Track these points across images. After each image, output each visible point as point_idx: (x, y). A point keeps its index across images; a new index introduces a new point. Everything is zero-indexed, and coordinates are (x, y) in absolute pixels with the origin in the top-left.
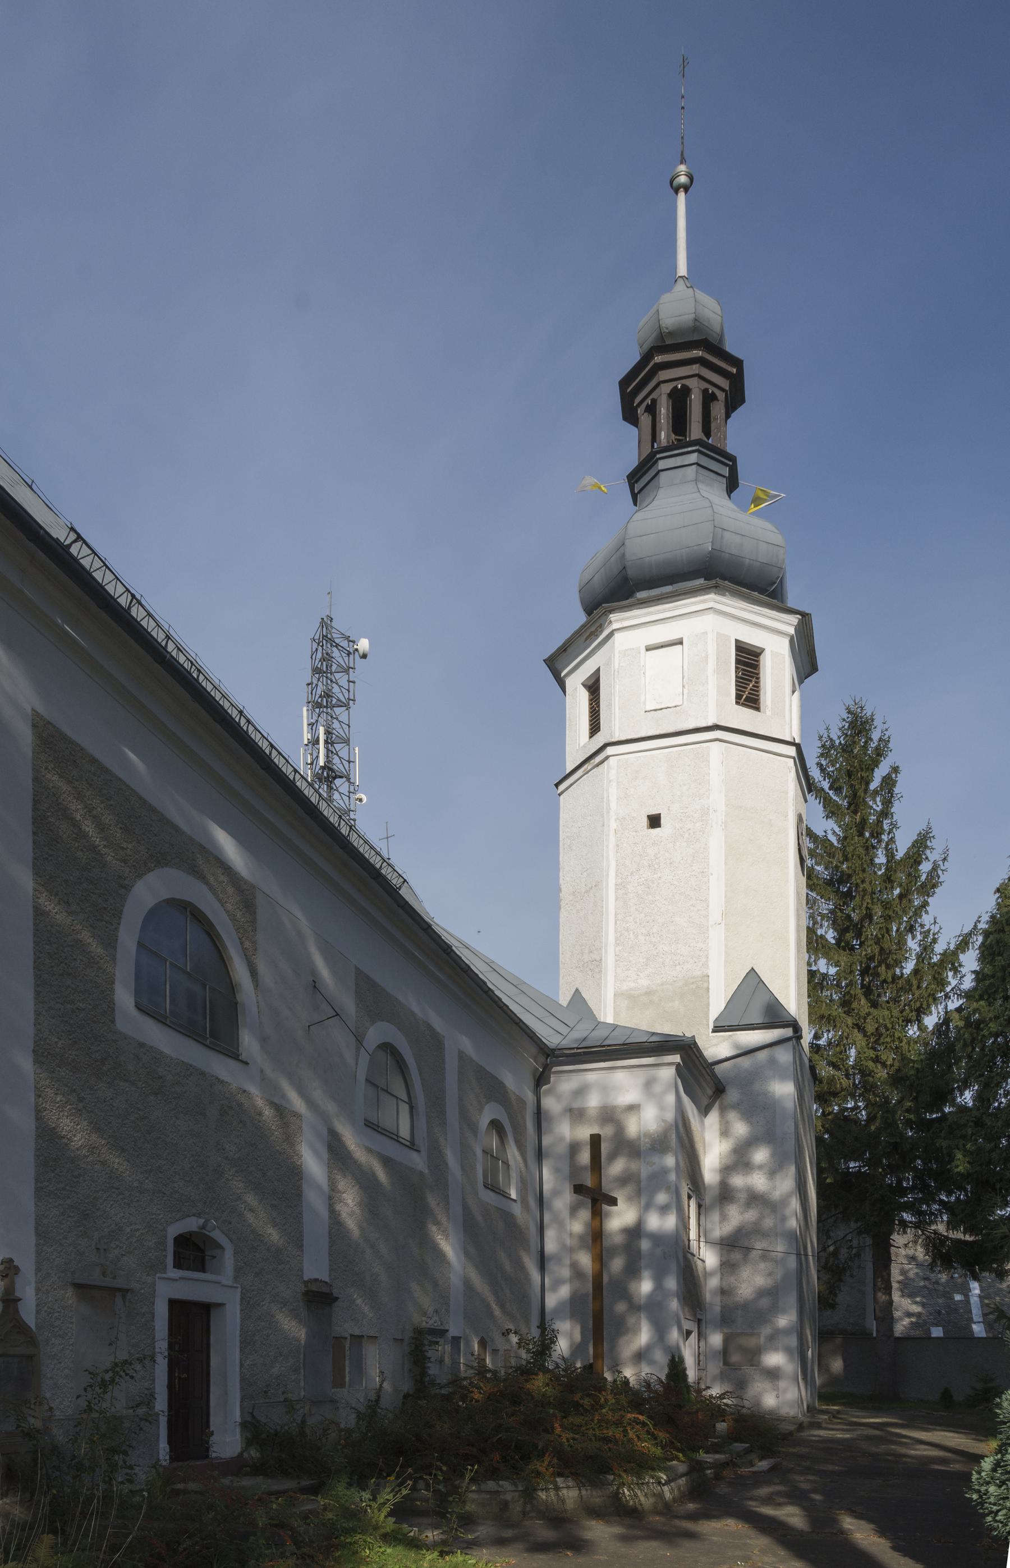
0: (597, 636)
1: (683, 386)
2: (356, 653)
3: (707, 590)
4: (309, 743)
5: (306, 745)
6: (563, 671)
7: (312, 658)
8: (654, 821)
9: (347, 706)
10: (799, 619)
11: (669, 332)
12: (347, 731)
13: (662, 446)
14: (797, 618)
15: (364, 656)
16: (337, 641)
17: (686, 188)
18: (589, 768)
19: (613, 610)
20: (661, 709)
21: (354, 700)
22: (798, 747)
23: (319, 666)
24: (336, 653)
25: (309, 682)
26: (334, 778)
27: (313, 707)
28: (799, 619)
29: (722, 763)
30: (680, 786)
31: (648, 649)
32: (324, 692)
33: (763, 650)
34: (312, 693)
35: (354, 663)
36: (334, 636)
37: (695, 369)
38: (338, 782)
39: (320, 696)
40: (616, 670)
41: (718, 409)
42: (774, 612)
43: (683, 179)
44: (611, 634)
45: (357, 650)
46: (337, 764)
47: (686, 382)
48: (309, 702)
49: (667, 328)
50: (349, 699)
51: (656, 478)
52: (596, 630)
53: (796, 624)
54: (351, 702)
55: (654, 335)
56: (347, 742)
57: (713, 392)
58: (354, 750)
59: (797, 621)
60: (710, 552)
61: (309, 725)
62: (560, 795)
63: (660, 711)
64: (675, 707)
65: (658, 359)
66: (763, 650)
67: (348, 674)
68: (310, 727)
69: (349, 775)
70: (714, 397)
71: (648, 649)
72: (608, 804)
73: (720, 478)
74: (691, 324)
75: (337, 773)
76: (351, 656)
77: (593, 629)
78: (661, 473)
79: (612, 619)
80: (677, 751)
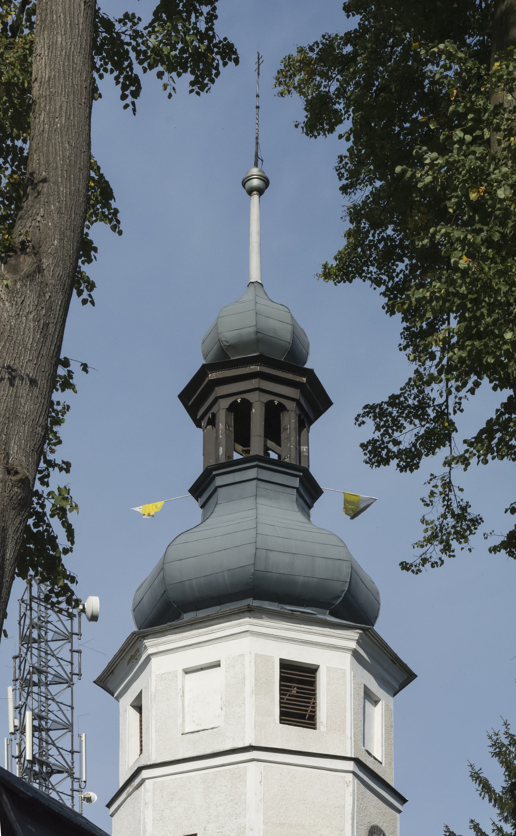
0: (138, 660)
1: (243, 400)
2: (83, 615)
3: (241, 615)
5: (12, 734)
6: (116, 691)
7: (20, 624)
9: (70, 683)
10: (360, 634)
11: (229, 345)
12: (68, 714)
13: (220, 462)
14: (358, 633)
15: (94, 618)
17: (260, 191)
18: (131, 790)
19: (147, 636)
20: (198, 731)
21: (79, 675)
22: (357, 761)
23: (28, 634)
24: (53, 617)
25: (17, 654)
28: (360, 634)
29: (260, 782)
30: (217, 806)
31: (187, 672)
32: (33, 667)
33: (318, 666)
34: (20, 668)
35: (80, 627)
37: (254, 383)
38: (55, 779)
39: (29, 673)
40: (153, 694)
42: (327, 630)
43: (256, 182)
44: (148, 659)
47: (246, 396)
48: (17, 680)
49: (227, 342)
50: (72, 674)
51: (215, 495)
52: (135, 654)
53: (357, 638)
54: (75, 678)
55: (216, 347)
56: (69, 727)
57: (279, 403)
58: (80, 736)
59: (358, 635)
60: (254, 574)
61: (16, 708)
62: (112, 815)
63: (197, 733)
64: (212, 728)
65: (212, 376)
66: (318, 666)
67: (71, 642)
68: (18, 711)
69: (72, 769)
70: (282, 408)
71: (187, 672)
72: (144, 823)
73: (289, 490)
74: (253, 337)
75: (54, 767)
76: (76, 620)
77: (132, 653)
78: (219, 490)
79: (146, 644)
80: (213, 773)
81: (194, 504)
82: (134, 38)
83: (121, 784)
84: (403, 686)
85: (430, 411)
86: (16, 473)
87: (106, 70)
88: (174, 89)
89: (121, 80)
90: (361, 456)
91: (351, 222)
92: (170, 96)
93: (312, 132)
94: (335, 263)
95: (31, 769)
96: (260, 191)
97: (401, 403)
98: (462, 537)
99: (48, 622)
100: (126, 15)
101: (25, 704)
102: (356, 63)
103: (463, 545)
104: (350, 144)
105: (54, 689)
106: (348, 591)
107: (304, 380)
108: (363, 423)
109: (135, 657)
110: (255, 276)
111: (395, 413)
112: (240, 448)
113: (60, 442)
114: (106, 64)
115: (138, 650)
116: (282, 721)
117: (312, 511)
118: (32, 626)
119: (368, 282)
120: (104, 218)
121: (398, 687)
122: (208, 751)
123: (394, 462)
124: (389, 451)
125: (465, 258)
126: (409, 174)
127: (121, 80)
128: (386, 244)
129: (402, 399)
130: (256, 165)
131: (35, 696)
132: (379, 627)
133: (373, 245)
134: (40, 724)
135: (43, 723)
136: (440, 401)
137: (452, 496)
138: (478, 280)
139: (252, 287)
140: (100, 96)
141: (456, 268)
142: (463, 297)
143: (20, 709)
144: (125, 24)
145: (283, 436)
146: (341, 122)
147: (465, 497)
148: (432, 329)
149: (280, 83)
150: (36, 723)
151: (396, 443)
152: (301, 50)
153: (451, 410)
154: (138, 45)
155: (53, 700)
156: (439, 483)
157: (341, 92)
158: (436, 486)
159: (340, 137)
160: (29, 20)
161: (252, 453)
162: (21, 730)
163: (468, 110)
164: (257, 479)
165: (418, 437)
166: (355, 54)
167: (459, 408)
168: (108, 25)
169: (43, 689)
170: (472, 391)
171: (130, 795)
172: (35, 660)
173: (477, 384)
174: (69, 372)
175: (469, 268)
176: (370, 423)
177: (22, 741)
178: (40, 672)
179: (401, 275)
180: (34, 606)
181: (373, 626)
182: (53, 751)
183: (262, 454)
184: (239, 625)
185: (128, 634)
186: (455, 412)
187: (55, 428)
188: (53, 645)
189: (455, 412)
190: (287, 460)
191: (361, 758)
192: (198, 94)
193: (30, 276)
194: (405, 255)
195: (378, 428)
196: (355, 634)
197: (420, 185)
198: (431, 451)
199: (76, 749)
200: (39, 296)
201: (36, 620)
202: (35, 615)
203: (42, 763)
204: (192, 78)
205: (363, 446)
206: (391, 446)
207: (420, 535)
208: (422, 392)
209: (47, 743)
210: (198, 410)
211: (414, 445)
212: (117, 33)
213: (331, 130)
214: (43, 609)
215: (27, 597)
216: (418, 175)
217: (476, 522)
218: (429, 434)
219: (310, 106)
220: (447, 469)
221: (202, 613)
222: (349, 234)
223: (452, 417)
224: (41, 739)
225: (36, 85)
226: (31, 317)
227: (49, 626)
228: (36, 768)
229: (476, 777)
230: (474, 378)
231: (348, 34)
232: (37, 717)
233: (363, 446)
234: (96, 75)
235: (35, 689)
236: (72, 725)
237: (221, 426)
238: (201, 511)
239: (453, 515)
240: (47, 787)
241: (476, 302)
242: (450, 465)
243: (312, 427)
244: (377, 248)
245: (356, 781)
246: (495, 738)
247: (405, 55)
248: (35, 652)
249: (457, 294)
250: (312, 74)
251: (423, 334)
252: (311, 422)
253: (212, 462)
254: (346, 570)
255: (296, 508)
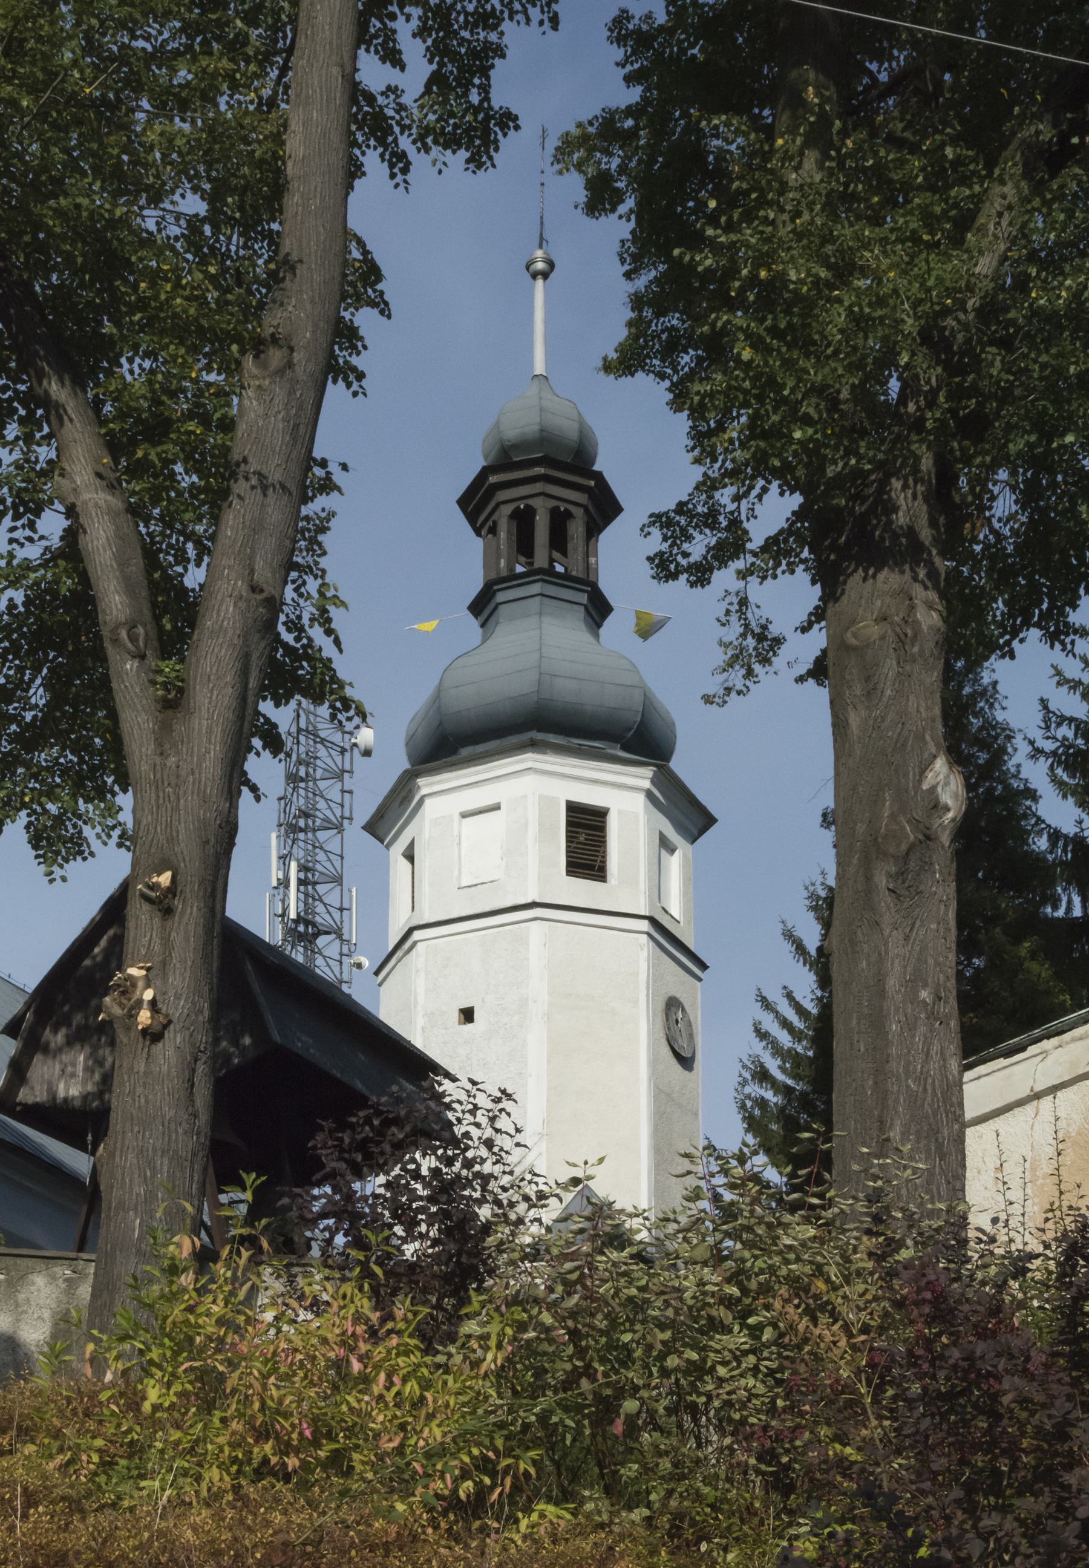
0: (410, 802)
1: (526, 506)
4: (279, 884)
8: (468, 1015)
9: (339, 828)
15: (367, 753)
16: (322, 734)
17: (545, 275)
21: (350, 819)
22: (652, 920)
24: (322, 752)
25: (282, 794)
26: (316, 935)
27: (286, 832)
31: (464, 815)
36: (320, 726)
37: (538, 487)
38: (321, 941)
41: (576, 529)
43: (540, 266)
45: (355, 745)
46: (322, 917)
47: (530, 502)
48: (280, 825)
50: (343, 817)
54: (346, 822)
55: (497, 447)
56: (338, 880)
58: (350, 891)
61: (280, 858)
62: (380, 985)
65: (493, 479)
67: (342, 781)
69: (340, 929)
70: (569, 515)
71: (464, 815)
73: (576, 607)
76: (347, 755)
77: (404, 794)
78: (502, 607)
81: (473, 623)
82: (397, 112)
83: (391, 947)
84: (702, 831)
85: (721, 518)
86: (262, 591)
87: (368, 146)
88: (445, 164)
89: (387, 157)
90: (647, 570)
91: (633, 310)
92: (440, 172)
93: (593, 213)
94: (615, 356)
95: (295, 929)
96: (545, 275)
97: (689, 511)
98: (765, 661)
99: (317, 758)
100: (389, 88)
101: (290, 853)
102: (638, 138)
103: (767, 668)
104: (632, 224)
105: (322, 835)
106: (642, 721)
107: (592, 483)
108: (649, 533)
109: (407, 798)
110: (539, 368)
111: (683, 522)
112: (523, 559)
113: (324, 553)
114: (368, 139)
115: (410, 791)
116: (569, 873)
117: (602, 631)
118: (299, 762)
119: (652, 376)
120: (373, 304)
121: (696, 832)
122: (487, 909)
123: (683, 577)
124: (678, 564)
125: (748, 349)
126: (687, 258)
127: (387, 157)
128: (670, 335)
129: (690, 506)
130: (541, 247)
131: (301, 844)
132: (676, 764)
133: (656, 336)
134: (306, 877)
135: (310, 875)
136: (732, 507)
137: (749, 615)
138: (762, 374)
139: (536, 381)
140: (364, 174)
141: (738, 359)
142: (746, 392)
143: (284, 859)
144: (388, 97)
145: (570, 546)
146: (623, 201)
147: (765, 613)
148: (721, 428)
149: (558, 162)
150: (302, 875)
151: (686, 555)
152: (579, 125)
153: (743, 517)
154: (402, 119)
155: (321, 848)
156: (735, 600)
157: (622, 169)
158: (731, 604)
159: (620, 217)
160: (285, 93)
161: (536, 566)
162: (284, 883)
163: (753, 189)
164: (541, 595)
165: (709, 549)
166: (636, 128)
167: (752, 515)
168: (370, 98)
169: (310, 835)
170: (760, 497)
171: (400, 960)
172: (302, 801)
173: (764, 490)
174: (328, 473)
175: (752, 361)
176: (656, 533)
177: (286, 895)
178: (306, 815)
179: (686, 369)
180: (302, 739)
181: (668, 759)
182: (320, 908)
183: (546, 565)
184: (522, 761)
185: (399, 773)
186: (748, 519)
187: (320, 538)
188: (322, 785)
189: (748, 519)
190: (574, 573)
191: (657, 917)
192: (474, 172)
193: (280, 372)
194: (690, 346)
195: (665, 539)
196: (648, 772)
197: (700, 269)
198: (723, 563)
199: (345, 905)
200: (290, 394)
201: (303, 756)
202: (302, 749)
203: (307, 923)
204: (468, 155)
205: (650, 559)
206: (679, 558)
207: (720, 657)
208: (711, 497)
209: (314, 899)
210: (477, 518)
211: (705, 558)
212: (380, 107)
213: (613, 210)
214: (311, 743)
215: (294, 729)
216: (697, 258)
217: (778, 641)
218: (720, 546)
219: (590, 185)
220: (742, 583)
221: (480, 748)
222: (630, 324)
223: (745, 525)
224: (306, 895)
225: (290, 164)
226: (280, 416)
227: (318, 762)
228: (301, 928)
229: (789, 935)
230: (760, 483)
231: (629, 107)
232: (303, 868)
233: (650, 559)
234: (357, 152)
235: (301, 836)
236: (341, 877)
237: (503, 535)
238: (480, 630)
239: (754, 635)
240: (313, 951)
241: (760, 399)
242: (744, 578)
243: (601, 536)
244: (660, 338)
245: (651, 943)
246: (811, 888)
247: (687, 130)
248: (302, 792)
249: (739, 389)
250: (591, 151)
251: (710, 433)
252: (600, 530)
253: (493, 575)
254: (638, 698)
255: (583, 627)
